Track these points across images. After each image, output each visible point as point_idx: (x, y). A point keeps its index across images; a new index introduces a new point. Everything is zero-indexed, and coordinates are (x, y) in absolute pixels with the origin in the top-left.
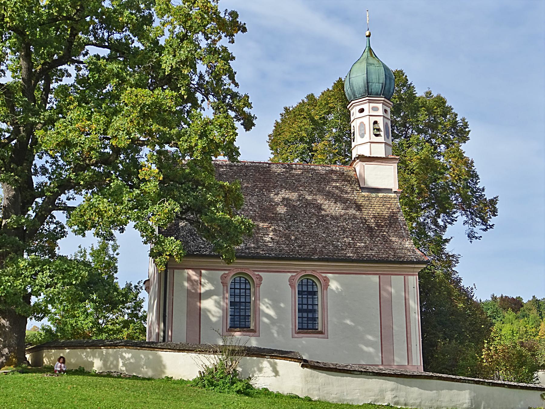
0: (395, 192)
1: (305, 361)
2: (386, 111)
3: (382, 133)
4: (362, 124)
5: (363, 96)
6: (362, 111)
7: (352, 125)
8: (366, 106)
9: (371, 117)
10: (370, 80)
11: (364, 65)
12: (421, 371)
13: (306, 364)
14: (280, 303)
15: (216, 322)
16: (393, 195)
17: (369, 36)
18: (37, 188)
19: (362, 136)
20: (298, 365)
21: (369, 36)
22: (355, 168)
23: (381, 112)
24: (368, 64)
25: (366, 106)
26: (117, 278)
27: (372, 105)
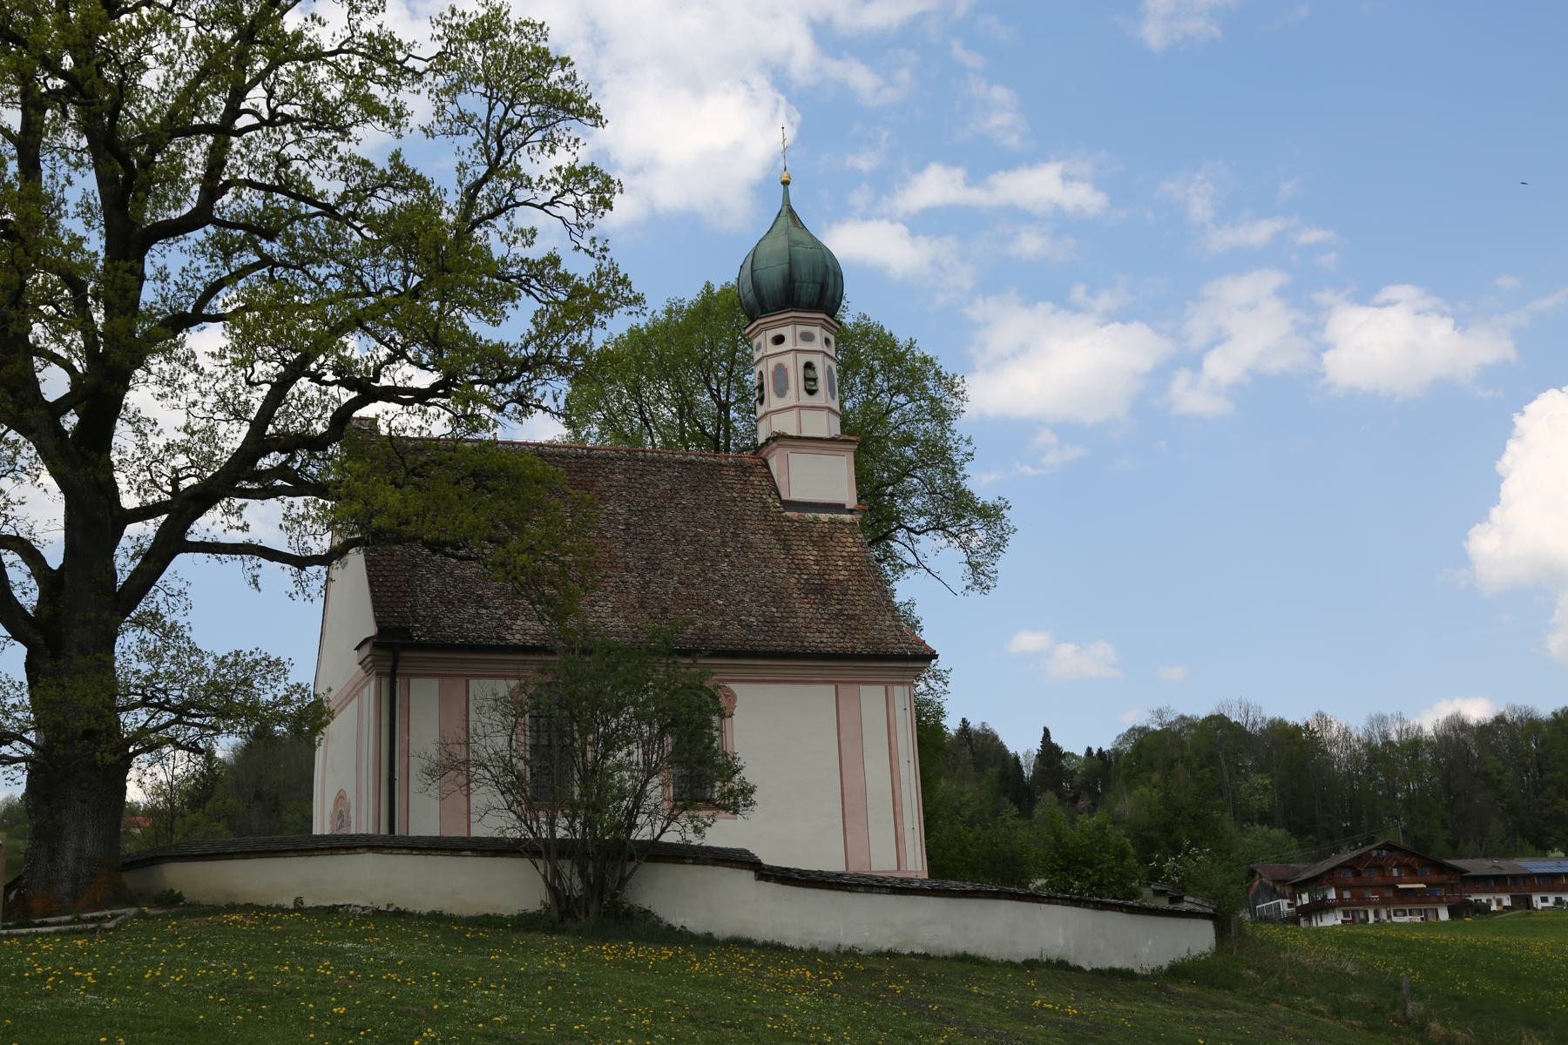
0: (851, 511)
2: (827, 341)
6: (779, 340)
8: (787, 331)
15: (134, 809)
16: (847, 518)
18: (224, 87)
19: (781, 393)
22: (766, 461)
23: (818, 344)
25: (787, 331)
26: (330, 690)
27: (800, 329)
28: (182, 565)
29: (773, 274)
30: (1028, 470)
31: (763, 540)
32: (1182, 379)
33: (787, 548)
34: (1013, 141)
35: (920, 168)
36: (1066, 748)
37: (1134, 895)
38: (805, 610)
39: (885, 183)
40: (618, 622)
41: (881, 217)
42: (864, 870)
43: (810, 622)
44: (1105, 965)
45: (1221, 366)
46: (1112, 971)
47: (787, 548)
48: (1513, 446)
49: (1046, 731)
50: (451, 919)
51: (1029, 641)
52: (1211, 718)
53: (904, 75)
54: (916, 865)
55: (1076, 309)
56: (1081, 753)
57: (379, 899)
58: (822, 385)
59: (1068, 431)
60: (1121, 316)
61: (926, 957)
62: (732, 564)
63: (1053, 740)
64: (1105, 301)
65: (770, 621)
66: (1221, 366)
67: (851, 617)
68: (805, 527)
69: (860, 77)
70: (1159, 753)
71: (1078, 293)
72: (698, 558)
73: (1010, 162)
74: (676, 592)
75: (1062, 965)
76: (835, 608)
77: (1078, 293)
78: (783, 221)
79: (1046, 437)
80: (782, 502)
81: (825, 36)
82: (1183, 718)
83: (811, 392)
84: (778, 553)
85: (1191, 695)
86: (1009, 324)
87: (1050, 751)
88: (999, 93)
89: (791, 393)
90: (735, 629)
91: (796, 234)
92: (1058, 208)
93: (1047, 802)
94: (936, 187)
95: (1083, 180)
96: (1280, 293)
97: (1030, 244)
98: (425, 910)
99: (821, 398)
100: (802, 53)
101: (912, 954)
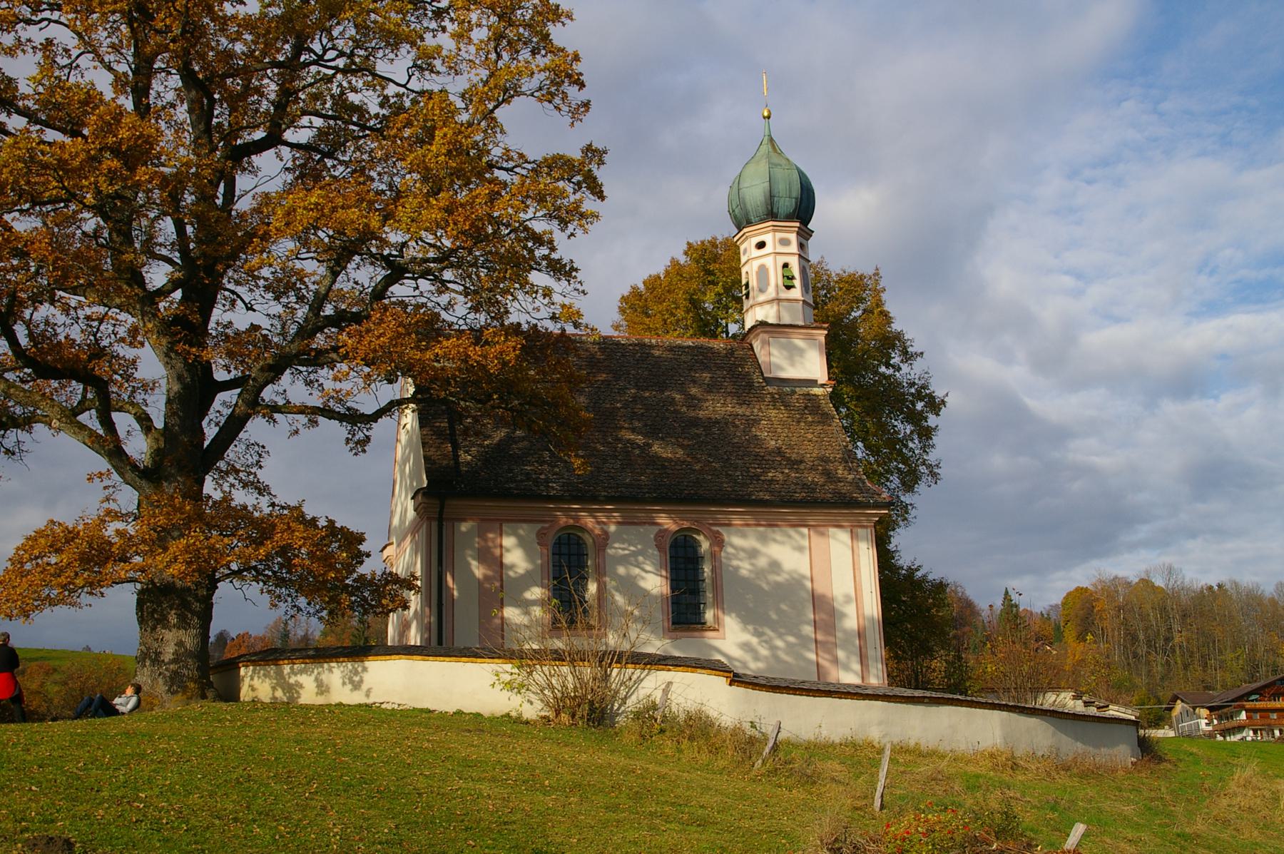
0: (822, 386)
1: (736, 675)
3: (797, 282)
4: (763, 270)
5: (762, 221)
6: (761, 245)
7: (744, 271)
8: (768, 238)
9: (778, 257)
10: (775, 192)
11: (763, 167)
13: (737, 679)
14: (502, 605)
17: (769, 117)
20: (720, 682)
21: (769, 117)
24: (772, 165)
27: (779, 235)
28: (256, 428)
57: (447, 704)
78: (766, 148)
80: (764, 379)
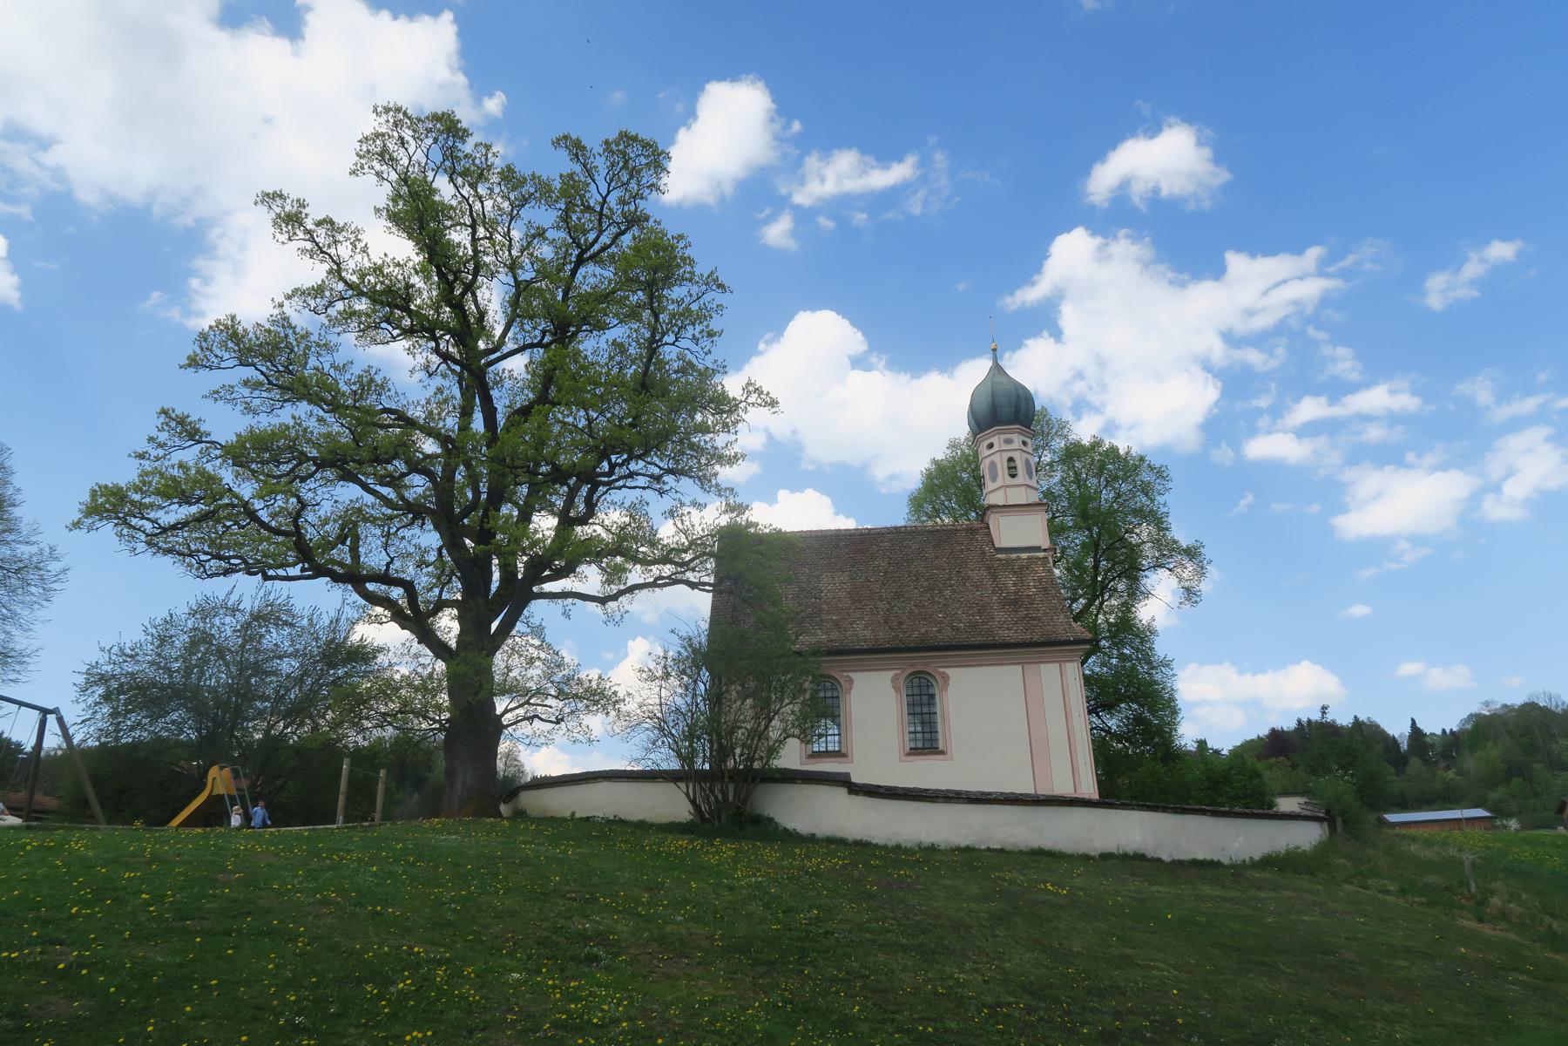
2: (1024, 443)
6: (991, 446)
12: (1096, 796)
16: (1041, 555)
19: (994, 479)
25: (995, 440)
29: (984, 407)
30: (1393, 566)
31: (977, 573)
32: (1489, 503)
33: (994, 577)
34: (1355, 377)
35: (1297, 400)
36: (1427, 731)
37: (1271, 805)
38: (1000, 615)
39: (1277, 412)
40: (868, 634)
41: (1278, 431)
42: (1049, 793)
43: (1003, 625)
44: (1188, 856)
45: (1516, 489)
46: (1195, 863)
47: (994, 577)
48: (427, 19)
49: (1413, 721)
50: (651, 825)
51: (1409, 669)
52: (1526, 705)
53: (1280, 351)
54: (1089, 788)
55: (1410, 467)
56: (1439, 732)
58: (1021, 470)
59: (1416, 540)
60: (1444, 467)
61: (1002, 851)
62: (953, 591)
63: (1419, 725)
64: (1429, 459)
65: (974, 626)
66: (1516, 489)
67: (1033, 619)
68: (1010, 563)
69: (1254, 357)
70: (1483, 729)
71: (1411, 457)
72: (931, 589)
73: (1354, 388)
74: (911, 611)
75: (1140, 857)
76: (1023, 613)
77: (1411, 457)
79: (1404, 545)
81: (1231, 339)
82: (1505, 706)
83: (1013, 476)
84: (988, 582)
85: (1513, 691)
86: (1368, 481)
87: (1416, 733)
88: (1341, 351)
89: (1000, 478)
90: (948, 632)
91: (998, 378)
92: (1389, 410)
93: (1415, 763)
94: (1310, 409)
95: (1403, 391)
96: (1549, 439)
97: (1375, 433)
98: (636, 819)
99: (1020, 479)
100: (1218, 351)
101: (989, 849)
